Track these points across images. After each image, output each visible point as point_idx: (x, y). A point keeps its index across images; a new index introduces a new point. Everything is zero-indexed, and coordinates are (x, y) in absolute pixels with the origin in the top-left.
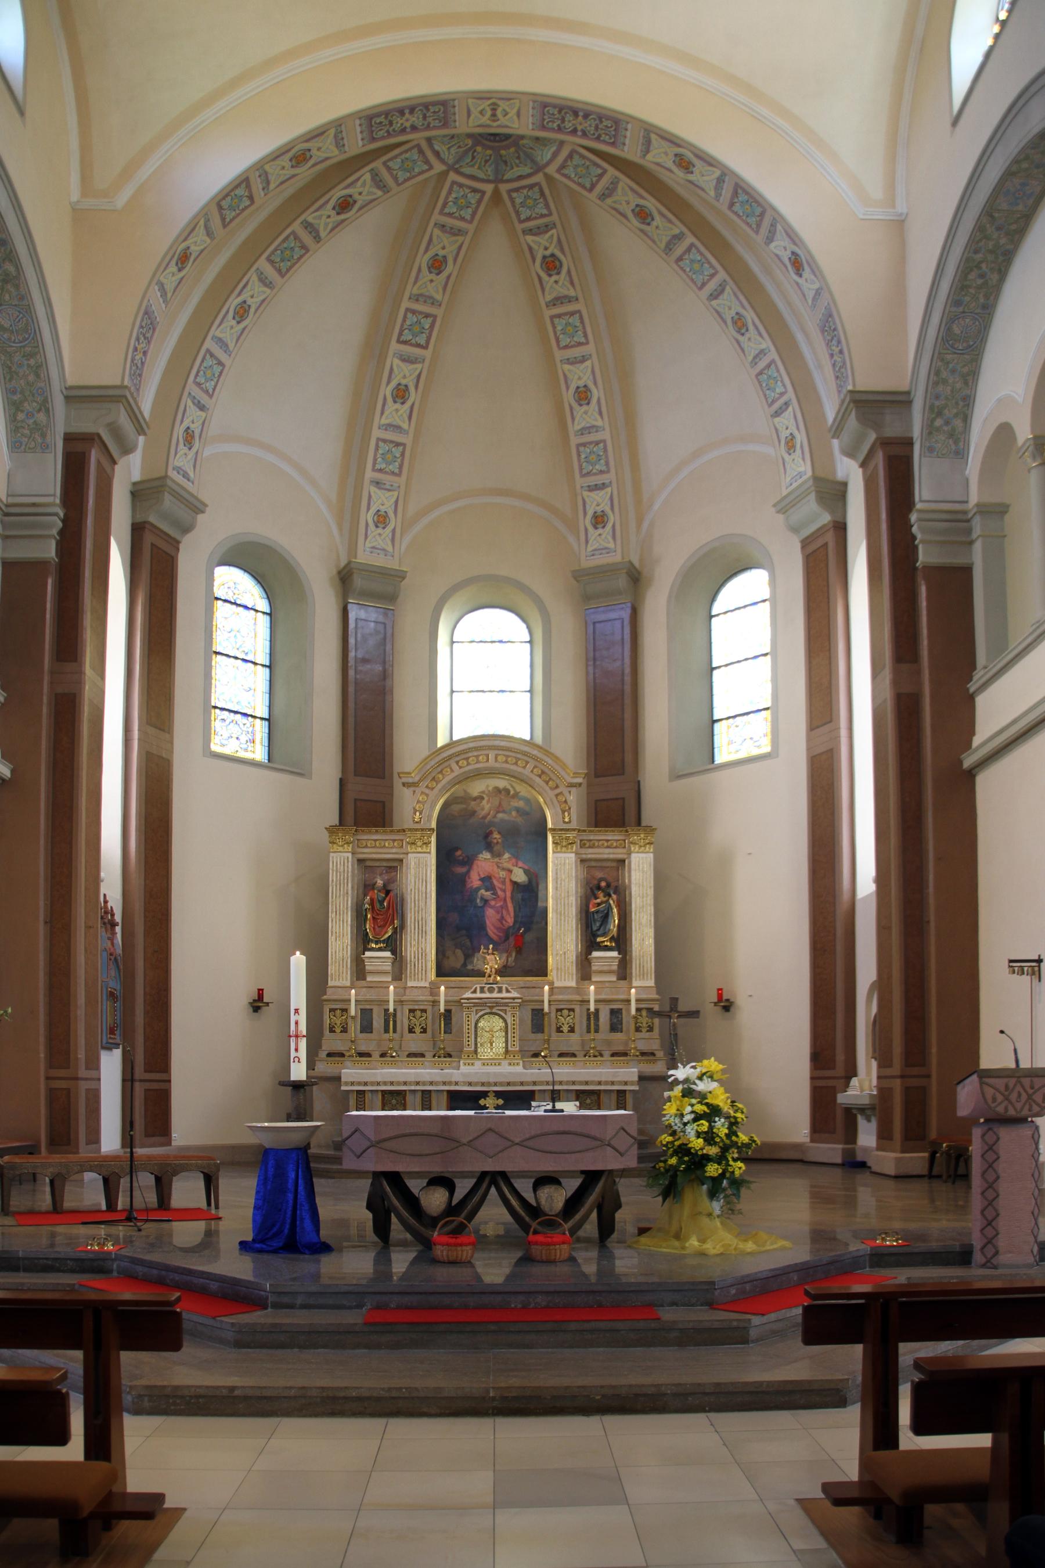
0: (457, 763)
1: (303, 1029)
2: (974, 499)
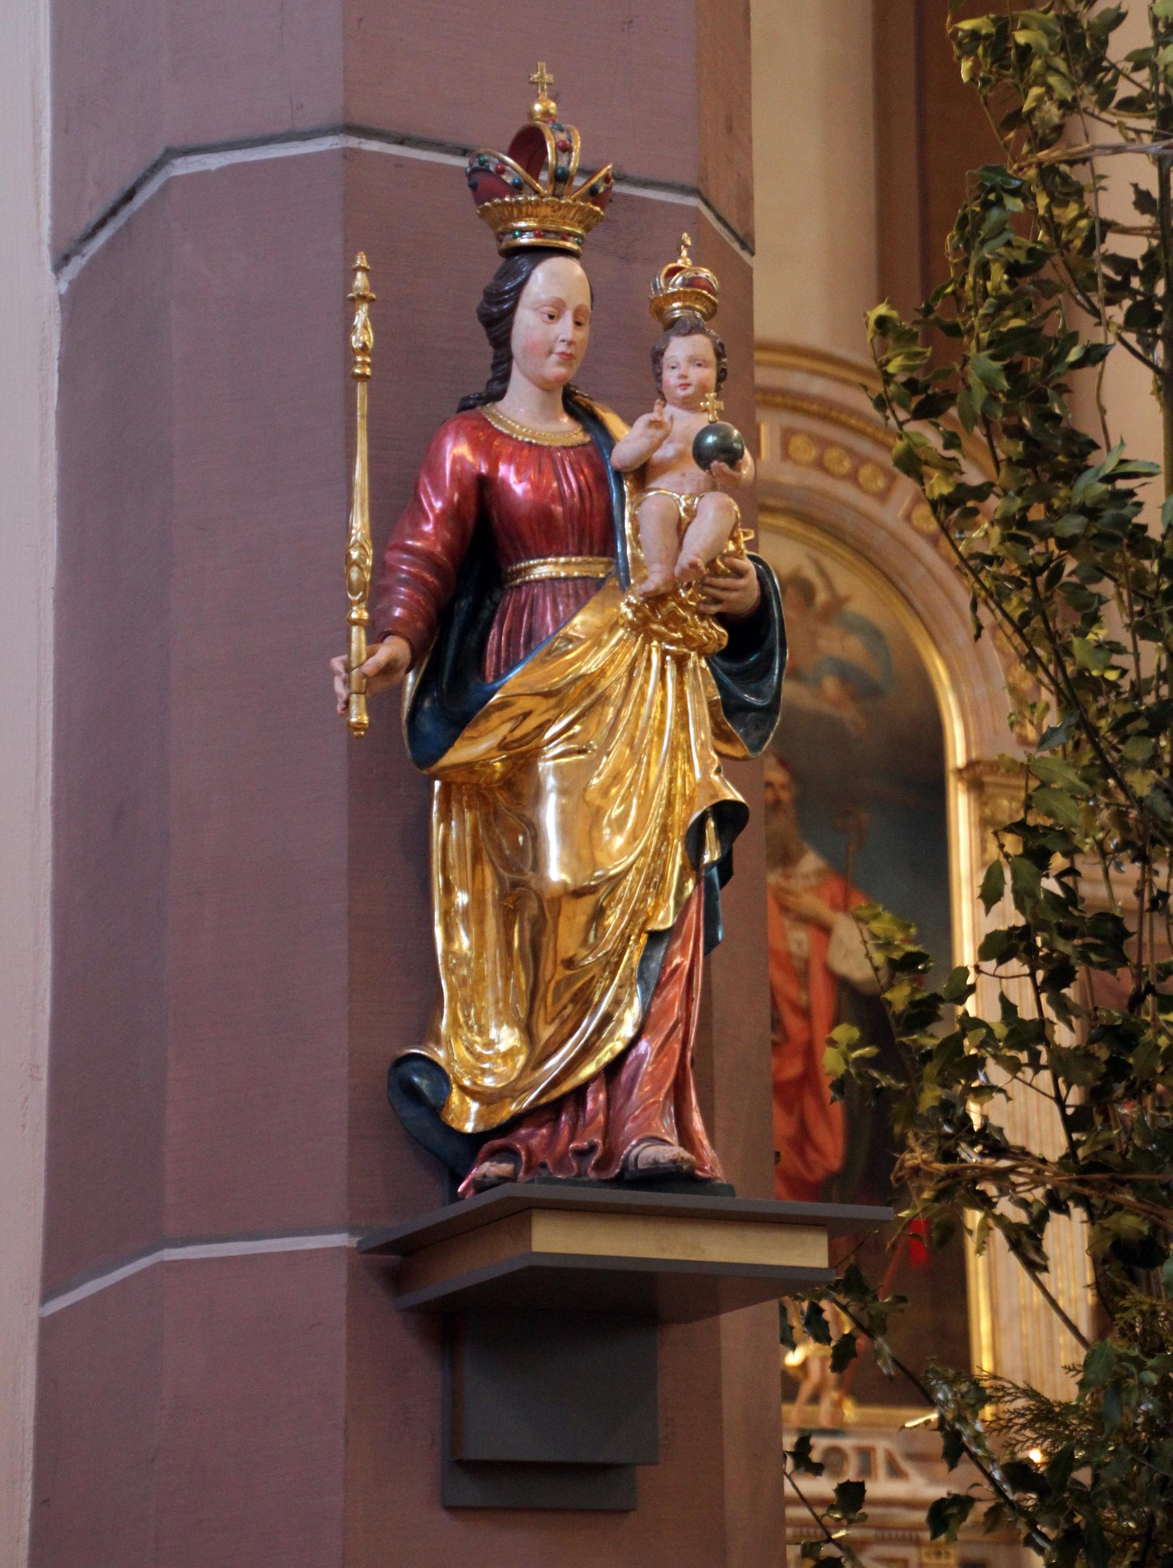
0: (787, 436)
1: (961, 808)
2: (341, 1240)
